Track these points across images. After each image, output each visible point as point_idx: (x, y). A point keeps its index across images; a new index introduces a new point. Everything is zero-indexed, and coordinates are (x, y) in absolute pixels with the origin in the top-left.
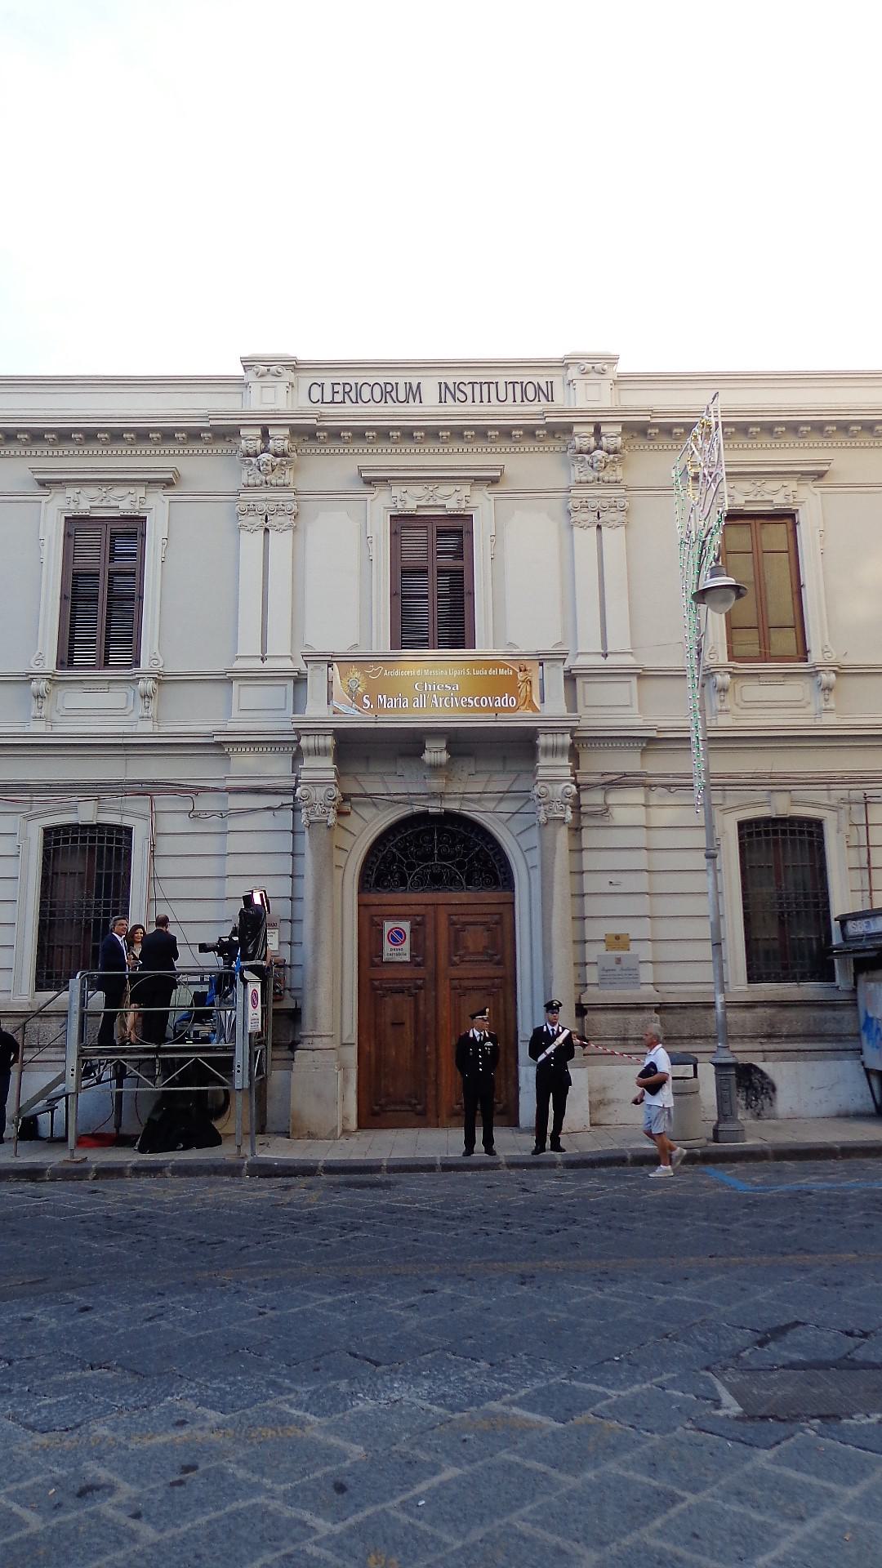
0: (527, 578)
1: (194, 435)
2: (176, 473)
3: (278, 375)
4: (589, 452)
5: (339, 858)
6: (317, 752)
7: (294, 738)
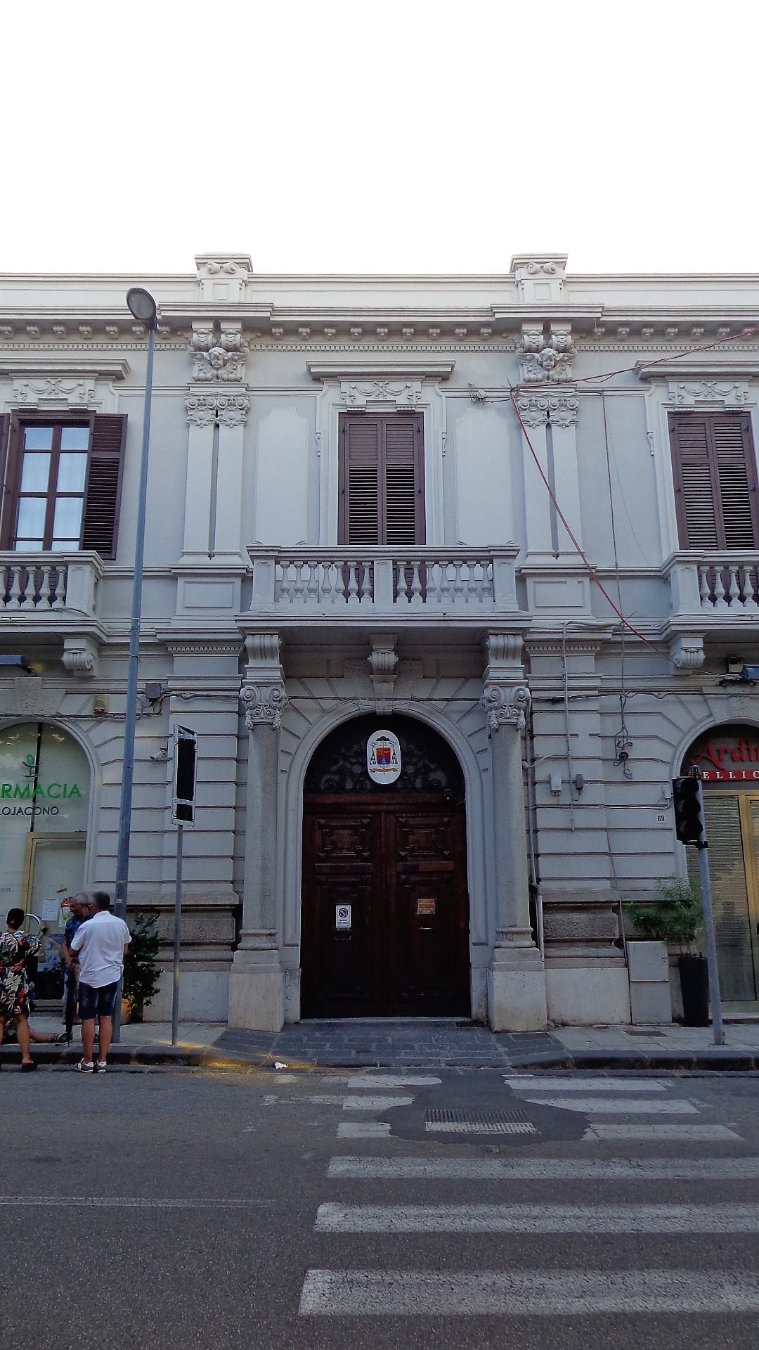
0: (475, 476)
1: (473, 330)
2: (125, 365)
3: (232, 272)
4: (538, 351)
5: (284, 762)
6: (263, 652)
7: (239, 636)
